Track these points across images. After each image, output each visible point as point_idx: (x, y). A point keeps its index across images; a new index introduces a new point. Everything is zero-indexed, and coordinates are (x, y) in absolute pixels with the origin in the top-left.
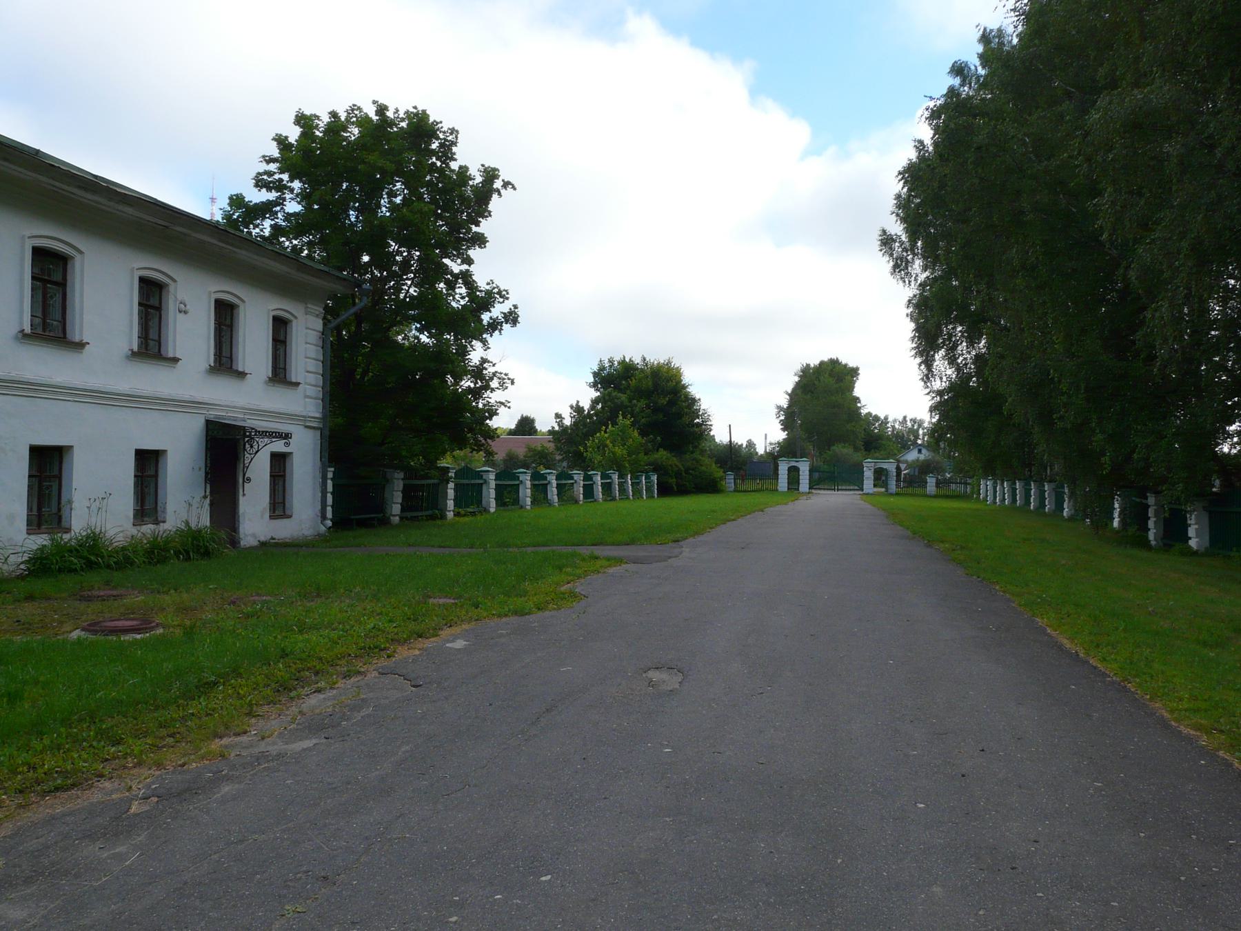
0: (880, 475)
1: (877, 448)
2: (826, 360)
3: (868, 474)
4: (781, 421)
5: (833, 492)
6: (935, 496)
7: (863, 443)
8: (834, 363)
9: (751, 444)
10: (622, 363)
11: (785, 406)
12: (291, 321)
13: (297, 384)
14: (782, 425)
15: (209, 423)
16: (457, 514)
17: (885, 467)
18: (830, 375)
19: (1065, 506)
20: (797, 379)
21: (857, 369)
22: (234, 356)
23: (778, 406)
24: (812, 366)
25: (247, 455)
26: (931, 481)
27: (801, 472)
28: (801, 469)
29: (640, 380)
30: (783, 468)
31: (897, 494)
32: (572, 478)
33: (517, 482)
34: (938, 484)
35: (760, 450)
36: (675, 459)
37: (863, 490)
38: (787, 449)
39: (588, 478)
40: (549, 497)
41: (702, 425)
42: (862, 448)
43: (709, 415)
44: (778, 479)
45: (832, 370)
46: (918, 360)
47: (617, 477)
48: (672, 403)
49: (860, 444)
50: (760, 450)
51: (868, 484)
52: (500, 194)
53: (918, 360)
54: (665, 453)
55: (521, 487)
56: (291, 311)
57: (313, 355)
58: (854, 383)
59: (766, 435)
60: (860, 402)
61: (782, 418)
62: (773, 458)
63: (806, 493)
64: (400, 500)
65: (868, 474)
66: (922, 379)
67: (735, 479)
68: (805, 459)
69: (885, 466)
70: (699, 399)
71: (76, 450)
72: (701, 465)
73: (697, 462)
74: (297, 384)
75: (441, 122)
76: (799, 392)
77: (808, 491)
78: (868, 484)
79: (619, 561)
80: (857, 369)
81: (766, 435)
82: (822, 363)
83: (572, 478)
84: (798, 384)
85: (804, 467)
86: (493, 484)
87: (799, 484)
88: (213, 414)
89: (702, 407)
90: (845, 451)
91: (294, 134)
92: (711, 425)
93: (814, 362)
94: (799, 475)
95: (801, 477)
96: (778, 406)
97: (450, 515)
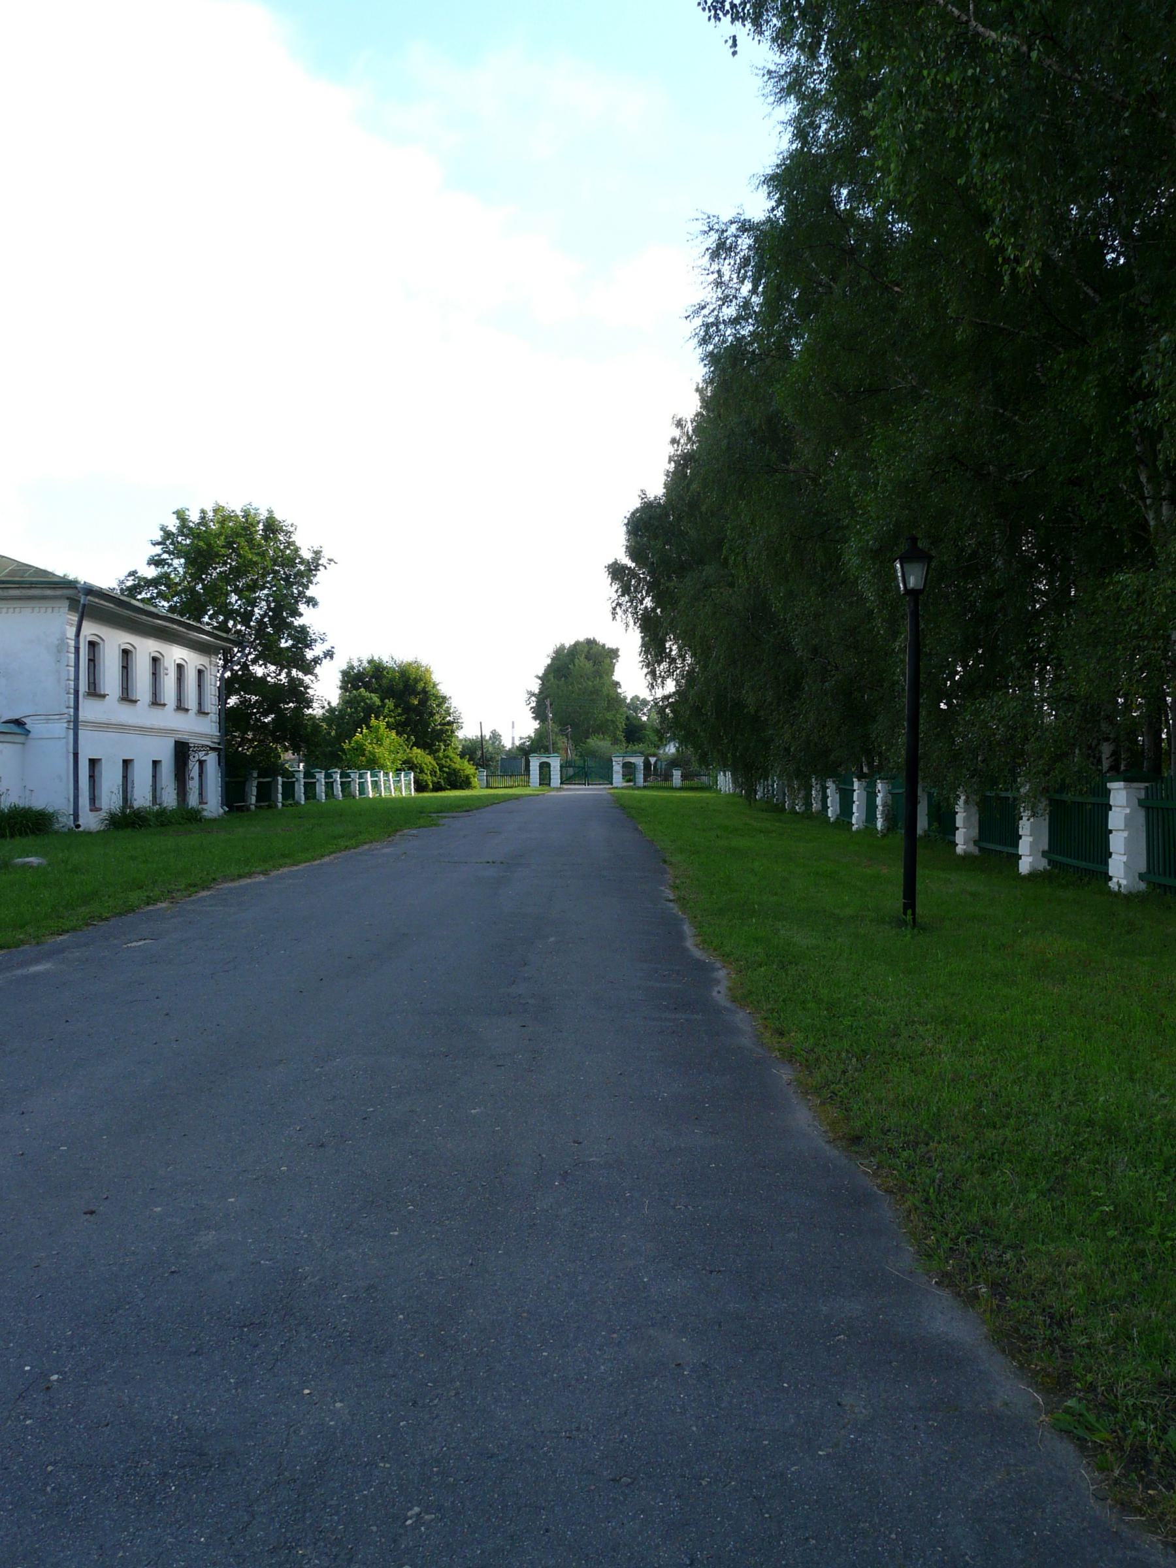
0: (629, 769)
1: (640, 740)
2: (581, 639)
3: (617, 768)
4: (532, 708)
5: (584, 786)
6: (681, 789)
7: (624, 734)
8: (591, 643)
9: (495, 736)
10: (371, 662)
11: (537, 691)
12: (98, 644)
13: (208, 714)
14: (533, 713)
15: (176, 742)
16: (283, 805)
17: (632, 761)
18: (586, 657)
19: (960, 820)
20: (549, 661)
21: (617, 650)
22: (97, 681)
23: (528, 692)
24: (567, 646)
25: (190, 762)
26: (677, 774)
27: (552, 769)
28: (552, 764)
29: (391, 681)
30: (535, 764)
31: (645, 787)
32: (350, 777)
33: (314, 780)
34: (684, 777)
35: (507, 743)
36: (429, 757)
37: (612, 784)
38: (538, 744)
39: (328, 776)
40: (335, 793)
41: (453, 723)
42: (624, 739)
43: (460, 713)
44: (529, 775)
45: (588, 652)
46: (645, 670)
47: (323, 776)
48: (423, 702)
49: (621, 735)
50: (507, 743)
51: (618, 779)
52: (326, 568)
53: (645, 670)
54: (419, 751)
55: (317, 784)
56: (102, 636)
57: (213, 693)
58: (614, 667)
59: (513, 723)
60: (620, 687)
61: (533, 704)
62: (524, 752)
63: (557, 788)
64: (255, 794)
65: (617, 768)
66: (648, 687)
67: (487, 776)
68: (556, 755)
69: (632, 760)
70: (450, 697)
71: (135, 762)
72: (455, 763)
73: (451, 760)
74: (208, 714)
75: (513, 738)
76: (551, 676)
77: (559, 786)
78: (618, 779)
79: (445, 817)
80: (617, 650)
81: (513, 723)
82: (577, 644)
83: (350, 777)
84: (549, 666)
85: (555, 763)
86: (302, 781)
87: (550, 779)
88: (179, 737)
89: (453, 705)
90: (601, 743)
91: (173, 525)
92: (462, 723)
93: (569, 642)
94: (550, 771)
95: (552, 773)
96: (528, 692)
97: (280, 805)
